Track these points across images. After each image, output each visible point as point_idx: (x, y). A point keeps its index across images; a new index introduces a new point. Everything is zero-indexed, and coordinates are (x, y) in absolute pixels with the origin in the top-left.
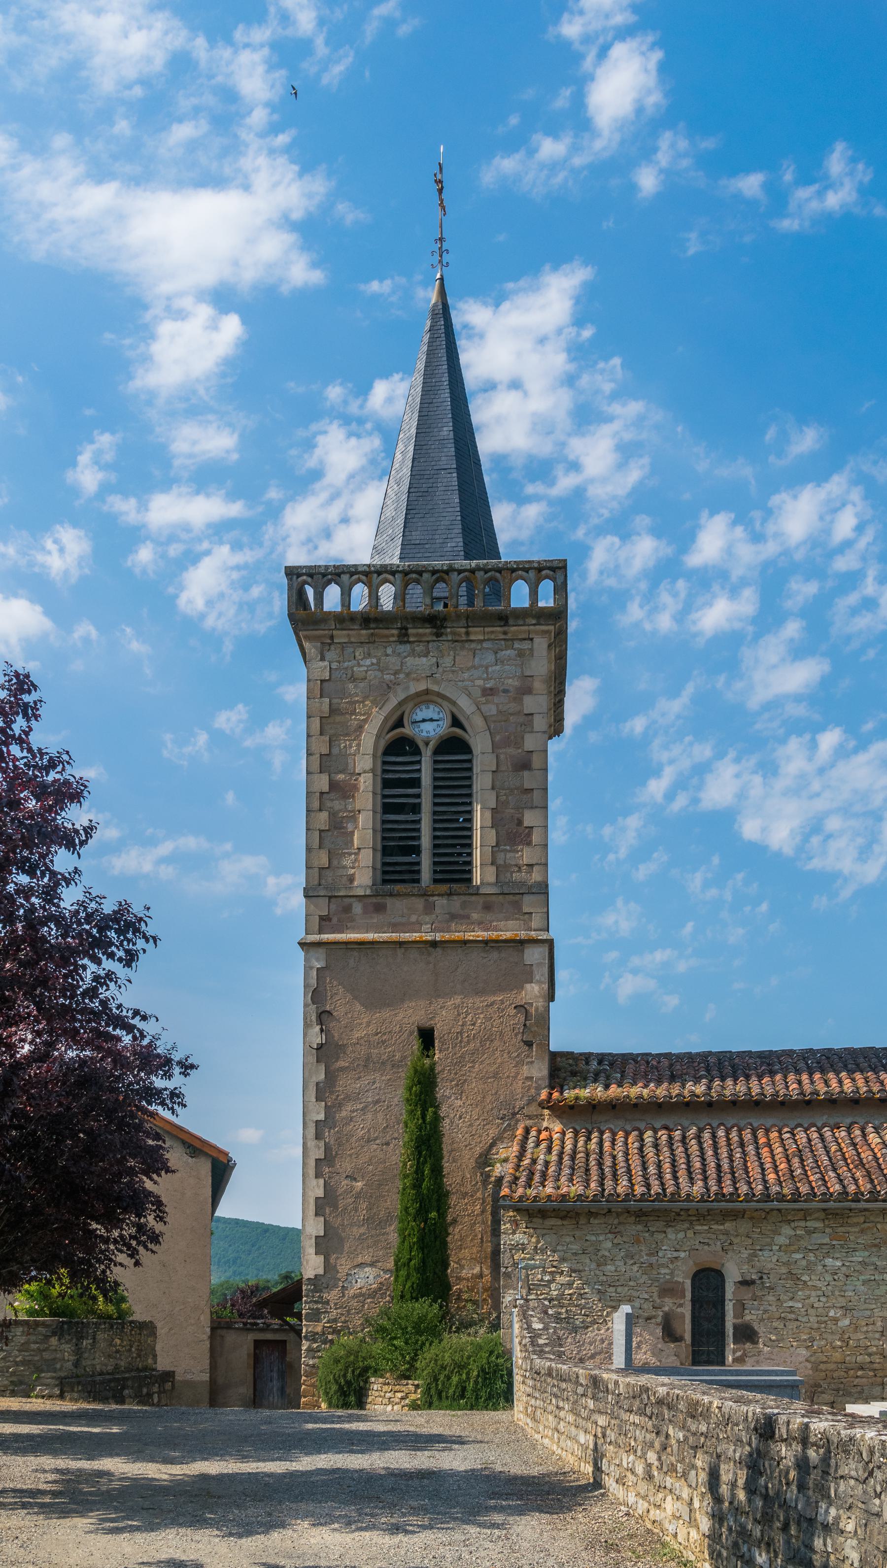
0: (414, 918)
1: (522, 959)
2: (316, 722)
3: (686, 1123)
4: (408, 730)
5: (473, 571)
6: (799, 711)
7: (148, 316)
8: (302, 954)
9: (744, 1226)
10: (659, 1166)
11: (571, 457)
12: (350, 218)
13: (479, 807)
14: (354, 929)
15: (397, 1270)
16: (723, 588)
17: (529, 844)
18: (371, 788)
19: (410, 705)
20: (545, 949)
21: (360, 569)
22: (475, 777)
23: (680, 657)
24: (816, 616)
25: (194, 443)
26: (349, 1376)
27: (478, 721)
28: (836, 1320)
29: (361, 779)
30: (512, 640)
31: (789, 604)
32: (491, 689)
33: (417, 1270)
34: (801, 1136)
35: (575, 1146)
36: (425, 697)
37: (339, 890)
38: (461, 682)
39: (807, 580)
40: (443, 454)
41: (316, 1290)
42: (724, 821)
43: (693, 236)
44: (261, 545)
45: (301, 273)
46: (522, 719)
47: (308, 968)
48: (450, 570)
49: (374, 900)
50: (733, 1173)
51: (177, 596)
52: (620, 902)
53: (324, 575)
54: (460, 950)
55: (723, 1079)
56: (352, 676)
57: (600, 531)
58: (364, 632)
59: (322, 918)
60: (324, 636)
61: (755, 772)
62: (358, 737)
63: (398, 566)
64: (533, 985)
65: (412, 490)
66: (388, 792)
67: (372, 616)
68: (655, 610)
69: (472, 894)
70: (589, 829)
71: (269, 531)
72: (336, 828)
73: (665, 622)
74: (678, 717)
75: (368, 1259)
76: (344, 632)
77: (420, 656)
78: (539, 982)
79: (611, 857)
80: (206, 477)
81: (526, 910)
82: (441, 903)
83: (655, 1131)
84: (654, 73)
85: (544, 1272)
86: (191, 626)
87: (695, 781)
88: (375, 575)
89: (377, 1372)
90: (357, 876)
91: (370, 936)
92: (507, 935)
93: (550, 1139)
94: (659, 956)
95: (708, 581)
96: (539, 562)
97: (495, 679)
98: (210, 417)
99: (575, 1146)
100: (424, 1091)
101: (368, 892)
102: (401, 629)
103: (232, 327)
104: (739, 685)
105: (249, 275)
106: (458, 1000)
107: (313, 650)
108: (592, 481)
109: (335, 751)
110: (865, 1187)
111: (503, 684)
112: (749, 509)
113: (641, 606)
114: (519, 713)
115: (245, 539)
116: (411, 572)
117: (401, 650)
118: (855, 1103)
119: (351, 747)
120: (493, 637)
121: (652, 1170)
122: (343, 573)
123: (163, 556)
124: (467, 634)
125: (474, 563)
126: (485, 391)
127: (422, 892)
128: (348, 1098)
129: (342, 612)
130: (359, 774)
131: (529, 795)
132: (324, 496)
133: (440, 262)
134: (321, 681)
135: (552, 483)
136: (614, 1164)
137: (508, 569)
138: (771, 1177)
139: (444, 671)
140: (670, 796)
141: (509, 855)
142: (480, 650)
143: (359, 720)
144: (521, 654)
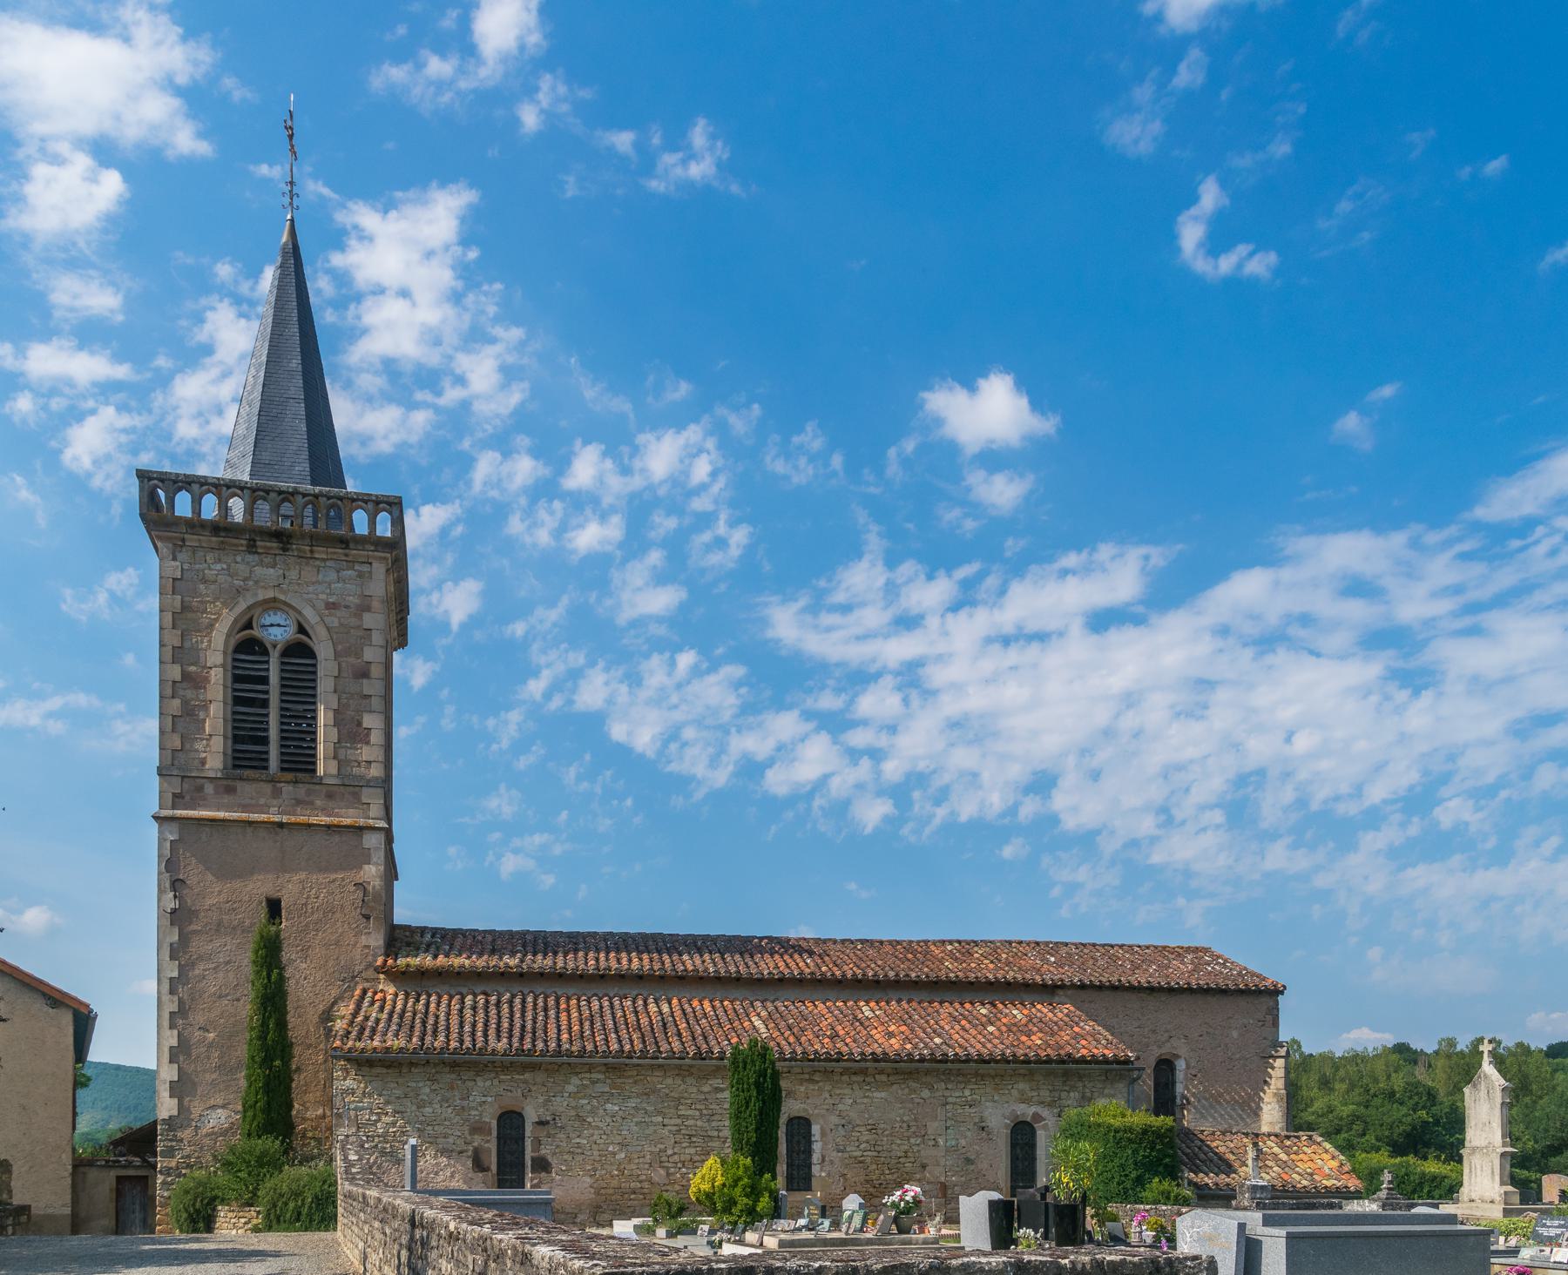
0: (262, 801)
1: (365, 842)
2: (169, 616)
3: (501, 990)
4: (256, 632)
5: (316, 496)
6: (661, 631)
7: (20, 154)
8: (156, 825)
9: (540, 1077)
10: (474, 1025)
11: (458, 371)
12: (237, 95)
14: (206, 807)
15: (245, 1111)
16: (594, 512)
17: (368, 743)
20: (381, 837)
23: (557, 567)
24: (676, 546)
25: (75, 297)
26: (198, 1205)
28: (614, 1154)
29: (213, 672)
31: (653, 534)
33: (263, 1111)
34: (595, 1004)
35: (405, 1006)
36: (272, 605)
38: (308, 597)
39: (668, 514)
41: (170, 1130)
42: (595, 722)
43: (571, 179)
44: (150, 411)
45: (186, 141)
46: (361, 633)
47: (161, 840)
48: (295, 493)
50: (534, 1033)
51: (60, 452)
52: (502, 788)
53: (175, 482)
55: (534, 955)
57: (486, 444)
61: (621, 682)
66: (238, 686)
68: (535, 525)
70: (475, 719)
71: (158, 399)
73: (543, 537)
74: (555, 625)
75: (220, 1101)
78: (376, 864)
79: (495, 747)
80: (89, 333)
82: (287, 789)
83: (475, 996)
84: (534, 13)
85: (372, 1113)
86: (76, 484)
87: (569, 684)
89: (223, 1201)
91: (221, 815)
92: (348, 821)
93: (384, 1000)
94: (538, 839)
95: (584, 504)
98: (92, 272)
99: (405, 1006)
100: (270, 954)
103: (112, 184)
104: (609, 602)
105: (131, 133)
106: (303, 875)
108: (477, 397)
109: (188, 644)
110: (638, 1046)
112: (620, 444)
113: (522, 520)
114: (359, 627)
115: (133, 403)
118: (640, 978)
121: (467, 1028)
123: (45, 408)
125: (317, 489)
126: (374, 293)
128: (200, 958)
132: (215, 372)
135: (439, 394)
136: (436, 1022)
138: (565, 1036)
140: (548, 695)
144: (361, 575)
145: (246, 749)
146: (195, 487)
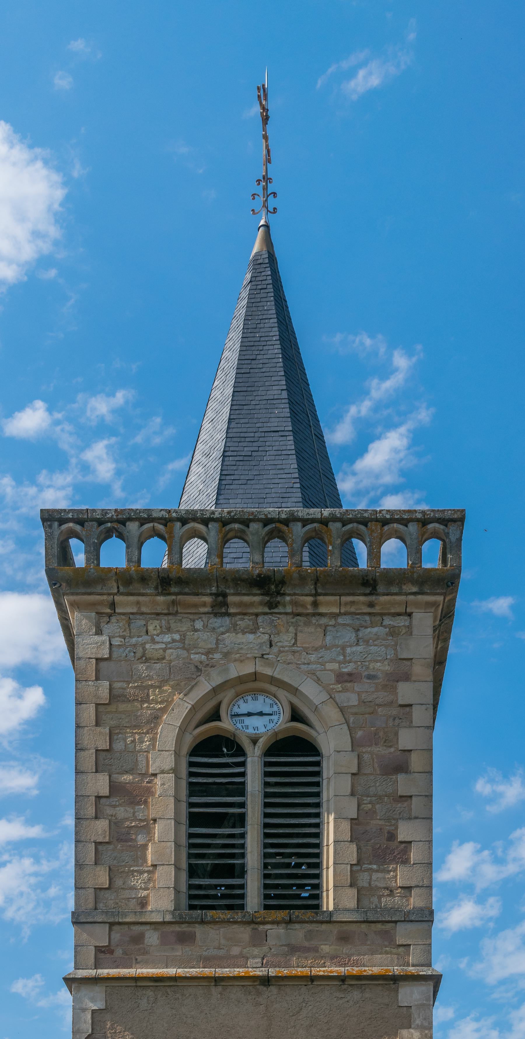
2: (90, 711)
4: (226, 724)
13: (332, 818)
14: (146, 964)
17: (405, 861)
18: (172, 792)
19: (230, 694)
21: (155, 515)
22: (325, 783)
27: (332, 714)
29: (158, 781)
30: (382, 615)
32: (350, 674)
36: (251, 684)
37: (125, 915)
38: (310, 669)
40: (272, 415)
46: (394, 711)
49: (177, 928)
53: (100, 522)
54: (304, 989)
56: (144, 655)
58: (161, 599)
59: (99, 950)
60: (101, 603)
62: (153, 730)
63: (213, 513)
64: (412, 1031)
65: (227, 454)
67: (173, 575)
69: (322, 922)
72: (119, 840)
76: (131, 598)
77: (244, 633)
81: (400, 940)
82: (276, 933)
88: (178, 524)
90: (151, 899)
91: (172, 971)
92: (376, 970)
96: (423, 512)
97: (356, 662)
98: (12, 763)
101: (168, 918)
102: (217, 595)
104: (479, 967)
107: (84, 622)
109: (118, 746)
111: (368, 668)
116: (233, 520)
117: (217, 625)
119: (142, 742)
120: (353, 610)
122: (130, 519)
124: (315, 604)
127: (247, 918)
129: (127, 570)
130: (155, 775)
131: (405, 804)
133: (265, 206)
134: (97, 659)
137: (377, 520)
139: (280, 652)
141: (375, 876)
142: (334, 626)
143: (154, 708)
144: (393, 632)
145: (210, 881)
146: (133, 527)
